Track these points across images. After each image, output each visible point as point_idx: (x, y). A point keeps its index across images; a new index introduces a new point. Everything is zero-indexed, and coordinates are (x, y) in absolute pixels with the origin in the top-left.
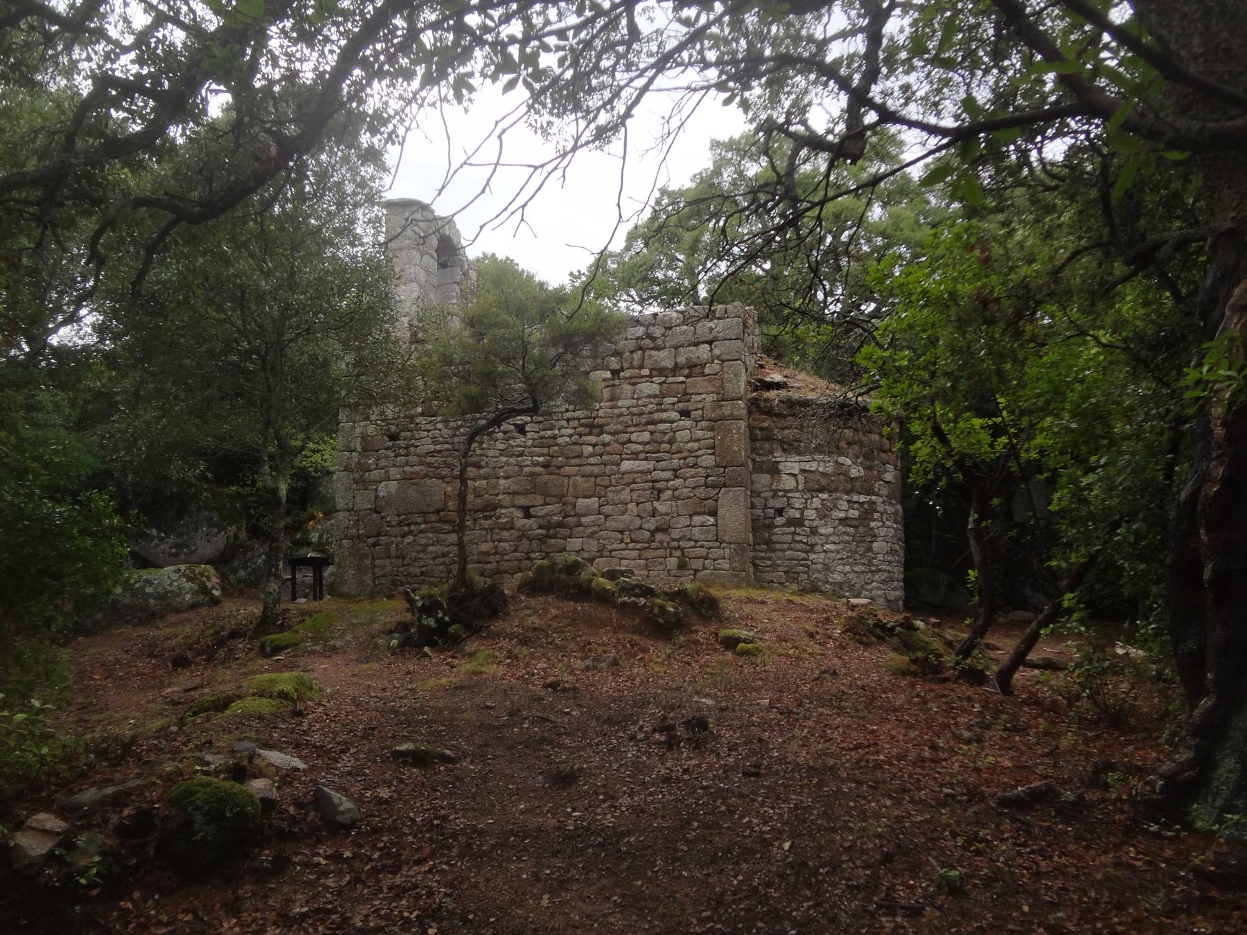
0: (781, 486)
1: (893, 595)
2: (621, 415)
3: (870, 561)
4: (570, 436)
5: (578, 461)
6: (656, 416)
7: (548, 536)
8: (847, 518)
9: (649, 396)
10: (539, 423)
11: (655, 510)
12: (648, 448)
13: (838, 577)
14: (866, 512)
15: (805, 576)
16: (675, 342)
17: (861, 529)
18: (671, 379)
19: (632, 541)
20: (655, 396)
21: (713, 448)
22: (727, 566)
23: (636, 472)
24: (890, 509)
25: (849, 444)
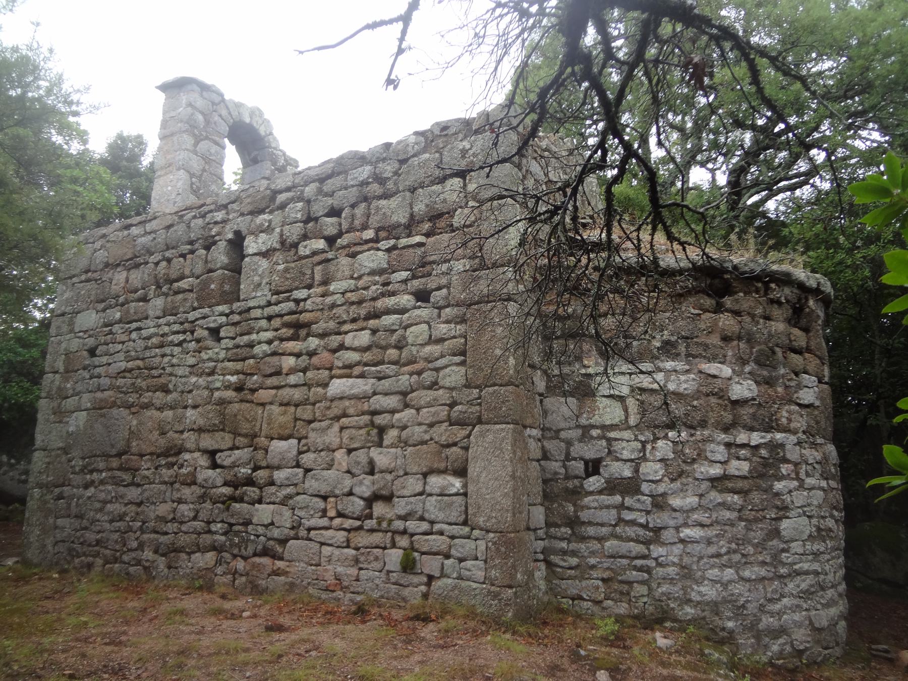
0: (596, 420)
1: (823, 617)
2: (333, 306)
3: (775, 557)
4: (269, 342)
5: (273, 381)
6: (380, 304)
7: (233, 499)
8: (725, 477)
9: (373, 273)
10: (235, 324)
11: (371, 463)
12: (367, 357)
13: (709, 592)
14: (765, 463)
15: (644, 590)
16: (410, 181)
17: (756, 497)
18: (403, 242)
19: (340, 515)
20: (381, 272)
21: (463, 353)
22: (480, 575)
23: (350, 398)
24: (813, 455)
25: (726, 339)
